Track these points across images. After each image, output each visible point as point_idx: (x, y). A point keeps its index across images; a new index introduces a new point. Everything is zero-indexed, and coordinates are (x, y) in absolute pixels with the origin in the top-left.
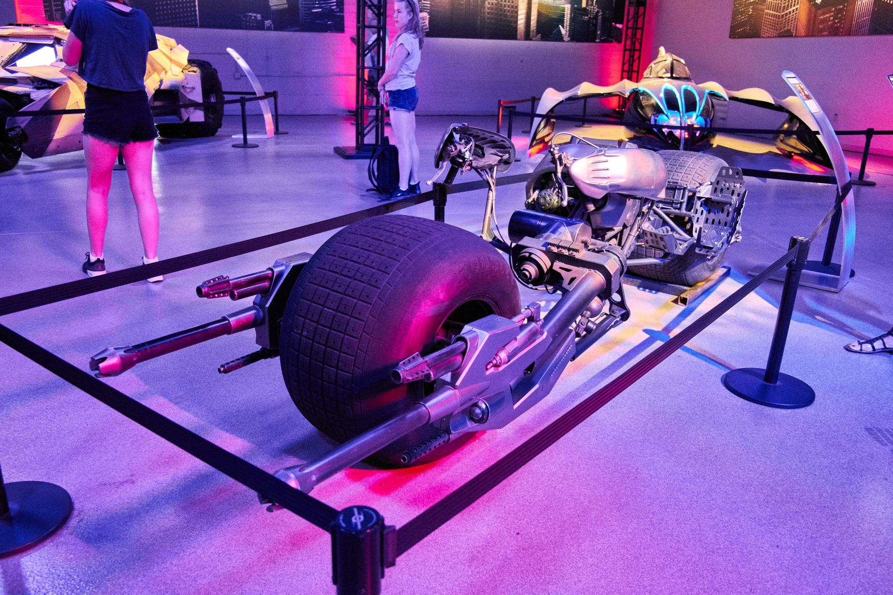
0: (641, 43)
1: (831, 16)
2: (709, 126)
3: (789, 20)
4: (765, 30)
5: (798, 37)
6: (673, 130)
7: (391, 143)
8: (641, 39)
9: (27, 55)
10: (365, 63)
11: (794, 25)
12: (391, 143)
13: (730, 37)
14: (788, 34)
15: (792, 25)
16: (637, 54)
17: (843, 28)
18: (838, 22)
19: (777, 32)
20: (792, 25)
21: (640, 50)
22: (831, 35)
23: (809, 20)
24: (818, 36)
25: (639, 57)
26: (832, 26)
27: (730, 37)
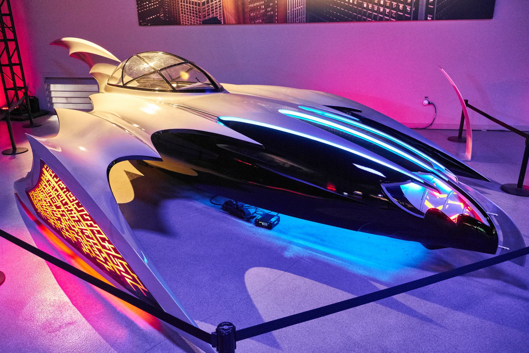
0: (14, 32)
1: (262, 5)
2: (41, 183)
3: (216, 8)
4: (183, 17)
5: (228, 24)
6: (15, 207)
7: (237, 343)
8: (13, 27)
9: (343, 150)
10: (463, 134)
11: (220, 12)
12: (237, 343)
13: (140, 24)
14: (215, 21)
15: (218, 12)
16: (12, 46)
17: (277, 16)
18: (271, 11)
19: (201, 20)
20: (218, 12)
21: (15, 40)
22: (266, 23)
23: (368, 15)
24: (251, 23)
25: (17, 48)
26: (265, 14)
27: (140, 24)
